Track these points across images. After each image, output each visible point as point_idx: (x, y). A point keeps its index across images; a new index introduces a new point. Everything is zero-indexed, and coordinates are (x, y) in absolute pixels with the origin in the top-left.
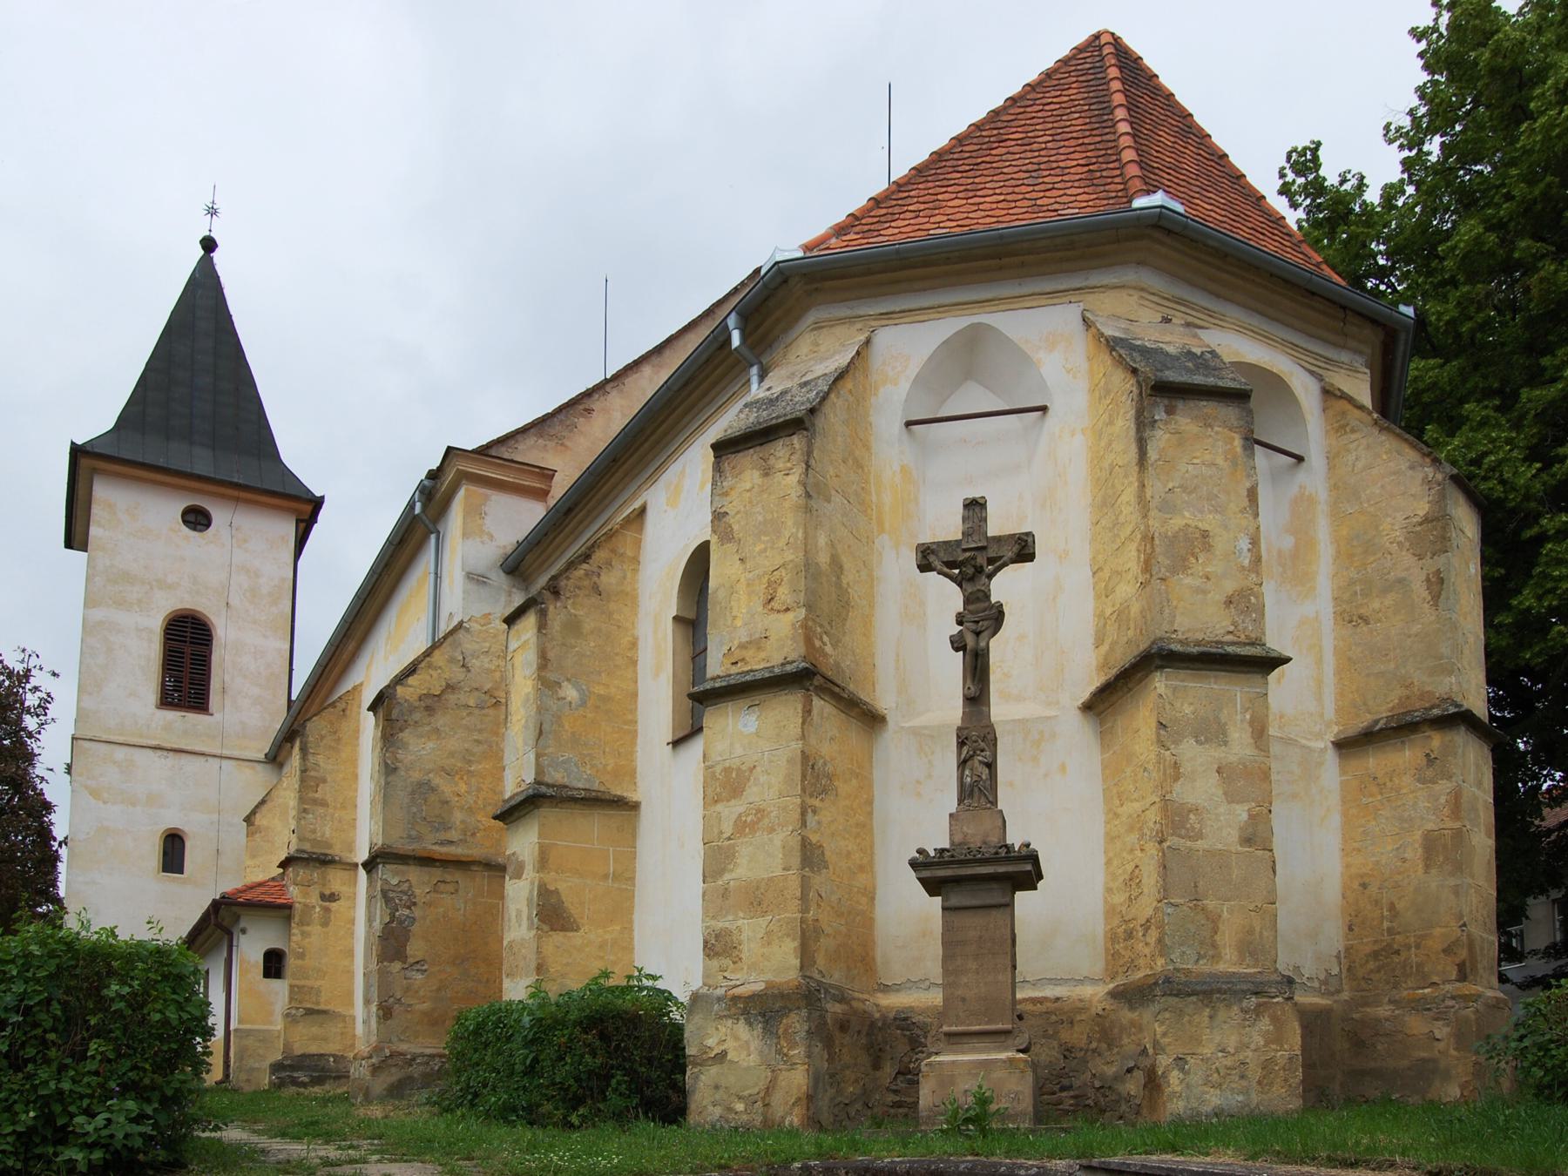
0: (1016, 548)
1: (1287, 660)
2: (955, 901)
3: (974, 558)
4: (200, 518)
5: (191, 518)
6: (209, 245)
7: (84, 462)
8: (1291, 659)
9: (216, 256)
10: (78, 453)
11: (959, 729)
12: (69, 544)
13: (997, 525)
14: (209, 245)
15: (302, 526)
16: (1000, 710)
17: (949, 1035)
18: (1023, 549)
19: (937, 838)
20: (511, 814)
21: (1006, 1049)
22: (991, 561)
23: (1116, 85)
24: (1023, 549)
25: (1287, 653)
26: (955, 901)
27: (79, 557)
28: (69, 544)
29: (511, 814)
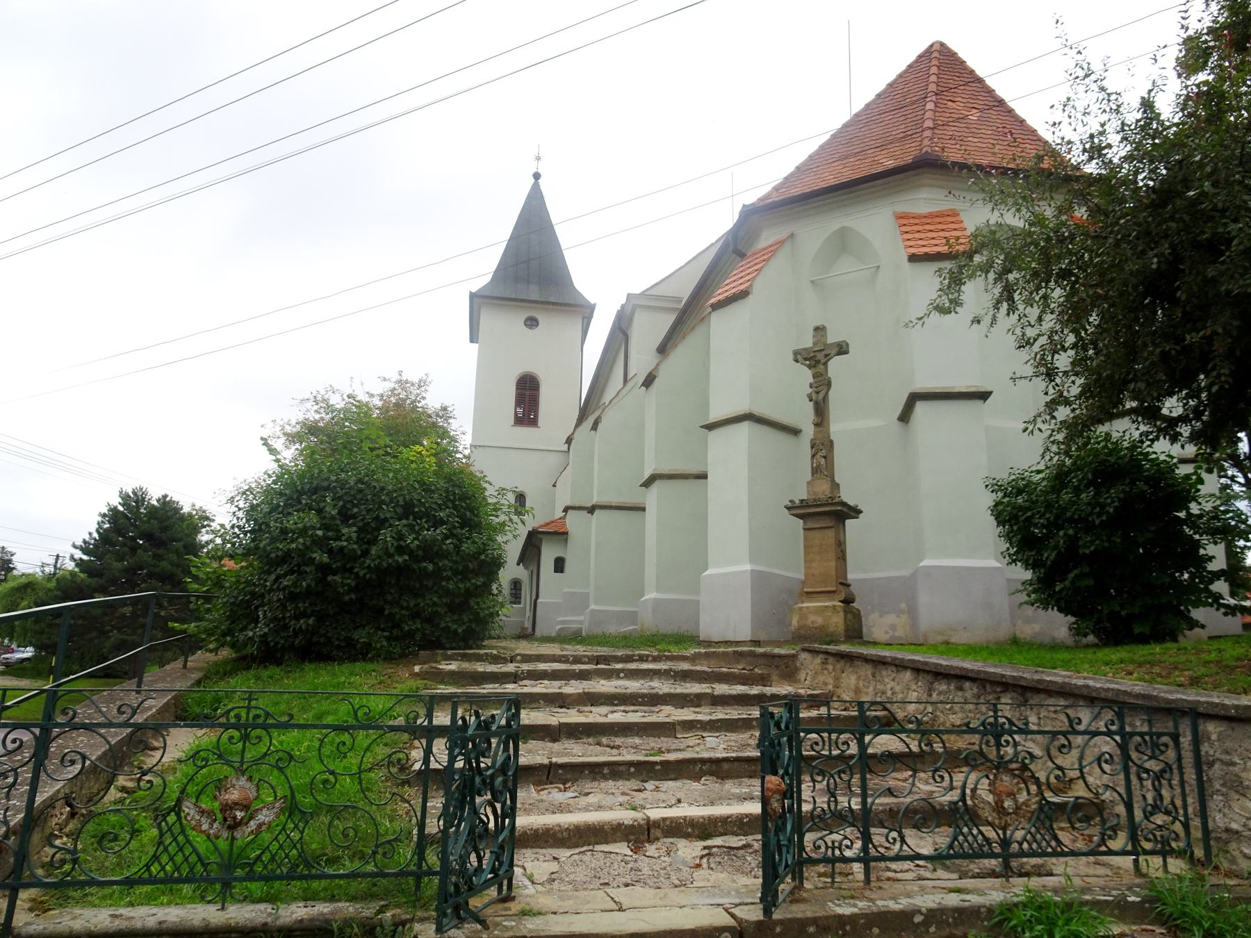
0: (837, 349)
1: (991, 393)
2: (810, 525)
3: (815, 356)
4: (534, 323)
5: (529, 323)
6: (537, 176)
7: (475, 300)
8: (991, 393)
9: (540, 181)
10: (473, 296)
11: (812, 440)
12: (472, 341)
13: (832, 338)
14: (537, 176)
15: (585, 321)
16: (837, 428)
17: (807, 593)
18: (842, 349)
19: (801, 494)
20: (647, 484)
21: (833, 600)
22: (826, 356)
23: (933, 78)
24: (842, 349)
25: (989, 389)
26: (810, 525)
27: (476, 346)
28: (472, 341)
29: (647, 484)
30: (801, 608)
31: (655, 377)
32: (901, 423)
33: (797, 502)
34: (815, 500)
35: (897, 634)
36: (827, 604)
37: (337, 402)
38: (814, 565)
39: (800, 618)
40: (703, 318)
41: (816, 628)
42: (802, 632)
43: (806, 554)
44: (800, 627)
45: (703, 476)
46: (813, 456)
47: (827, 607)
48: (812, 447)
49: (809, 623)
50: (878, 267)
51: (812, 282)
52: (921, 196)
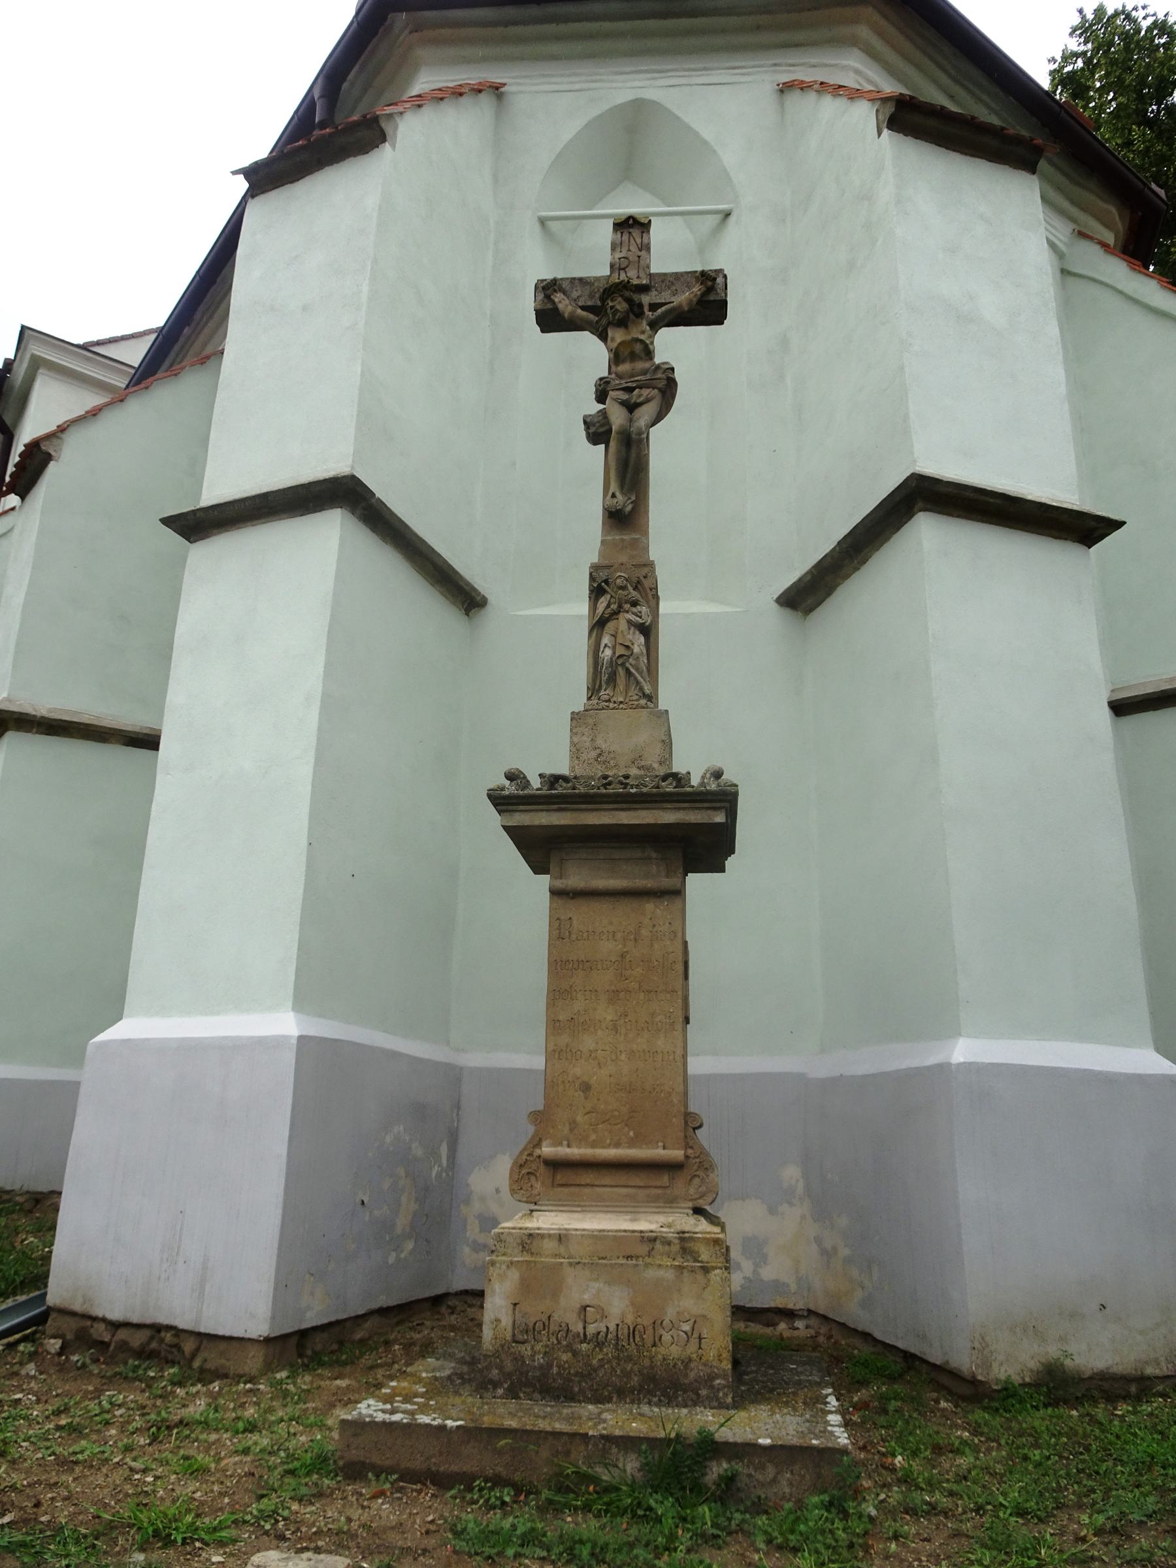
2: (576, 879)
8: (1123, 523)
11: (595, 568)
17: (556, 1165)
21: (670, 1202)
26: (576, 879)
30: (529, 1240)
31: (48, 458)
32: (787, 612)
33: (536, 783)
34: (606, 781)
35: (768, 1273)
36: (647, 1223)
37: (1095, 1370)
38: (588, 1042)
39: (526, 1286)
40: (208, 357)
41: (598, 1341)
42: (533, 1353)
43: (558, 994)
44: (526, 1332)
45: (149, 742)
46: (599, 625)
47: (650, 1240)
48: (597, 591)
49: (565, 1313)
50: (727, 215)
51: (542, 221)
52: (845, 62)
